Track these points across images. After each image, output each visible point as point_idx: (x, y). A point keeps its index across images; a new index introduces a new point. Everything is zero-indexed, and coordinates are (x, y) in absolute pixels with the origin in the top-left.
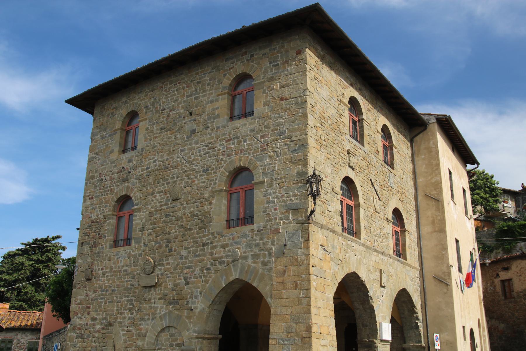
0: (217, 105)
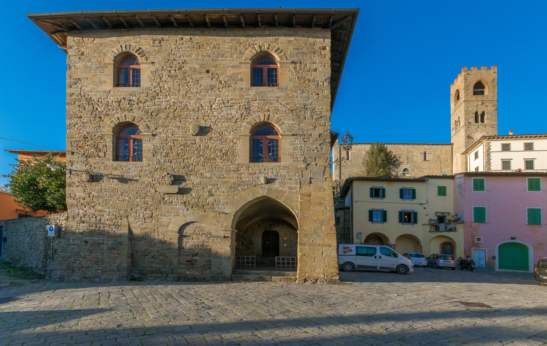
0: (240, 71)
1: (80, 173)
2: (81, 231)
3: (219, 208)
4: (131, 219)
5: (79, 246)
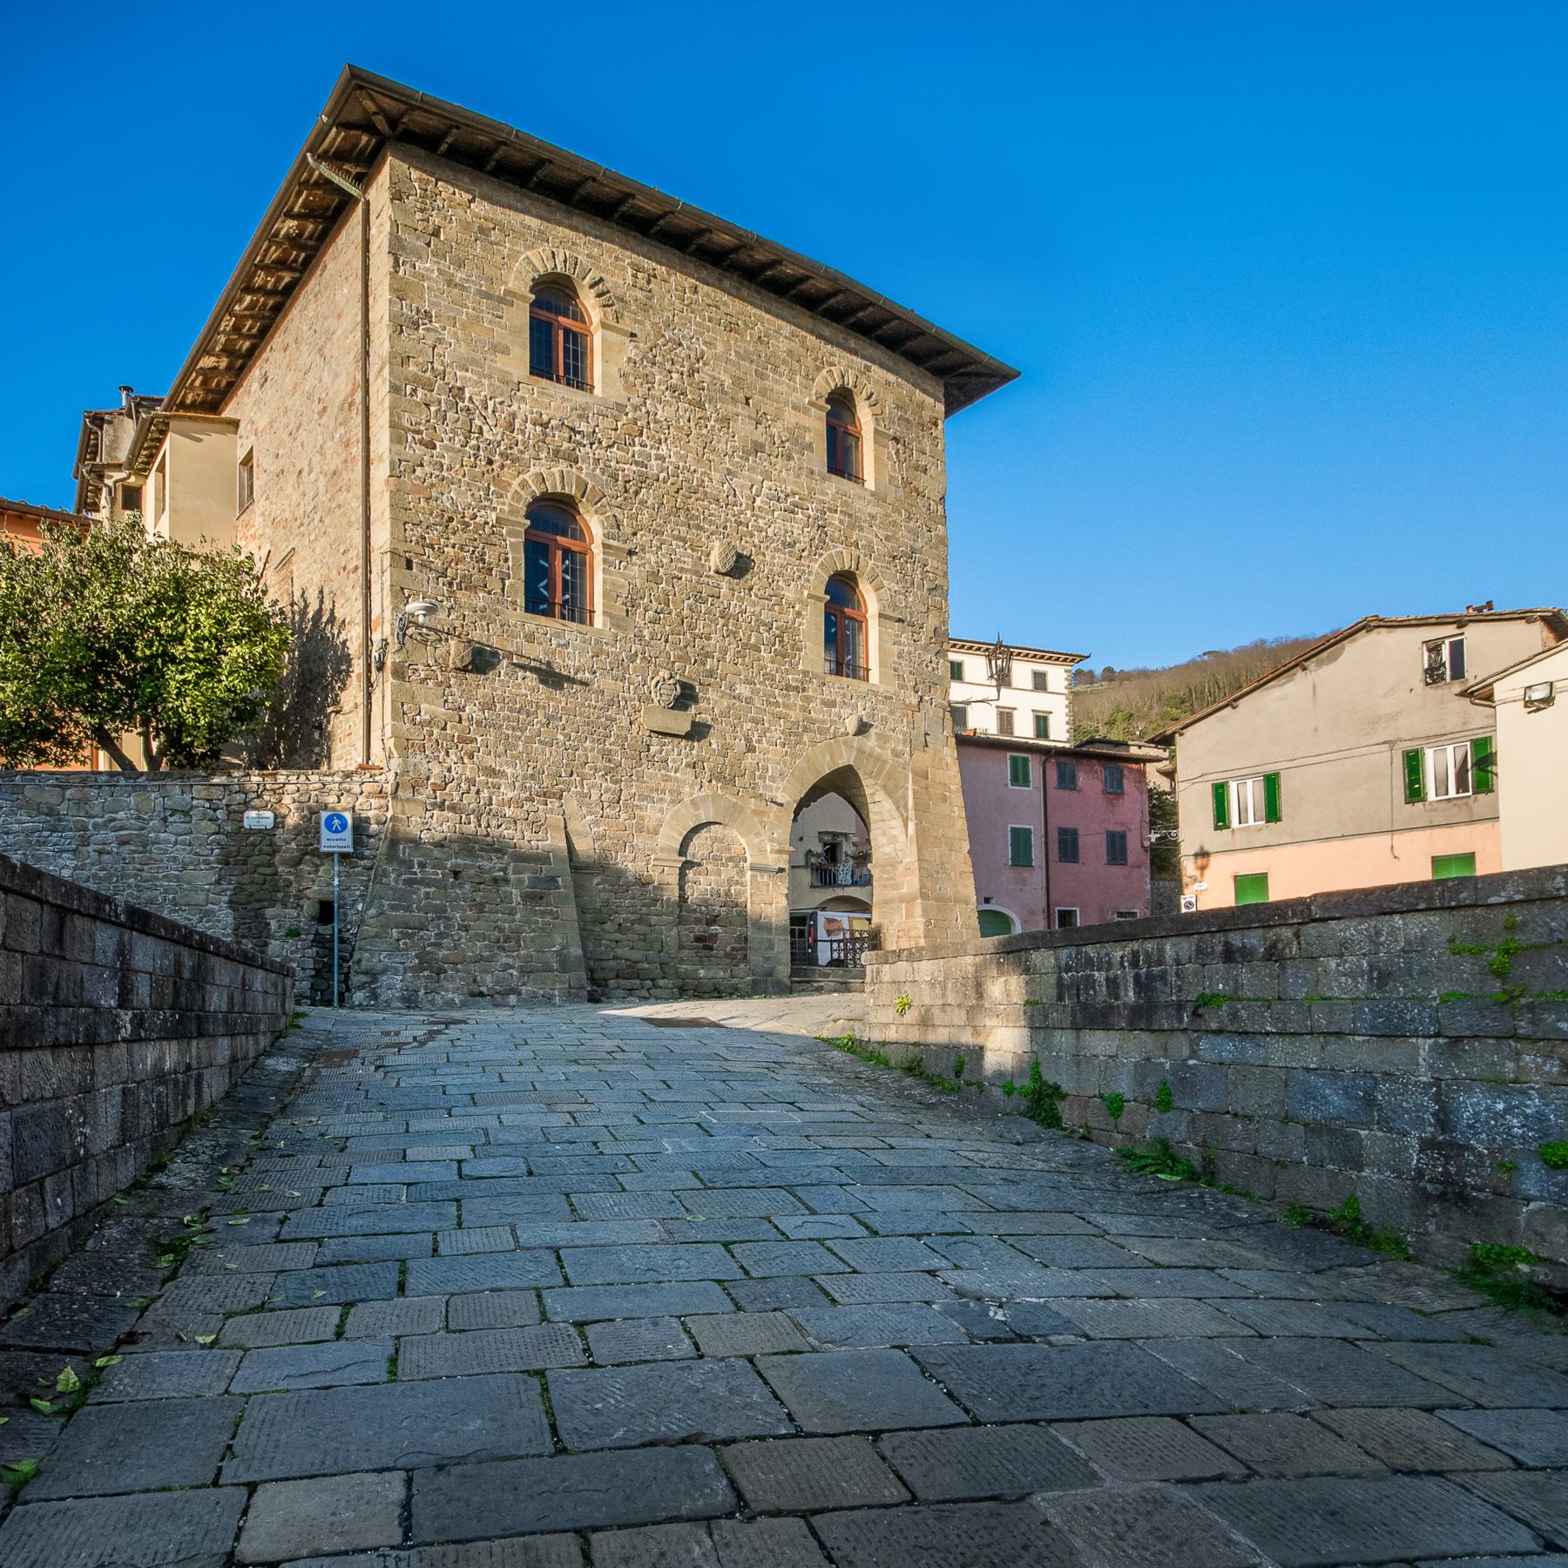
1: (433, 636)
2: (438, 837)
3: (765, 787)
4: (571, 803)
5: (441, 885)
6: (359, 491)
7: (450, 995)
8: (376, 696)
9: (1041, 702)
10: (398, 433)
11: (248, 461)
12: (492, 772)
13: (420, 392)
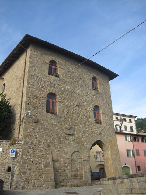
3: (85, 144)
6: (21, 91)
7: (30, 187)
8: (21, 127)
9: (131, 125)
10: (28, 83)
11: (4, 85)
12: (39, 142)
13: (32, 77)
